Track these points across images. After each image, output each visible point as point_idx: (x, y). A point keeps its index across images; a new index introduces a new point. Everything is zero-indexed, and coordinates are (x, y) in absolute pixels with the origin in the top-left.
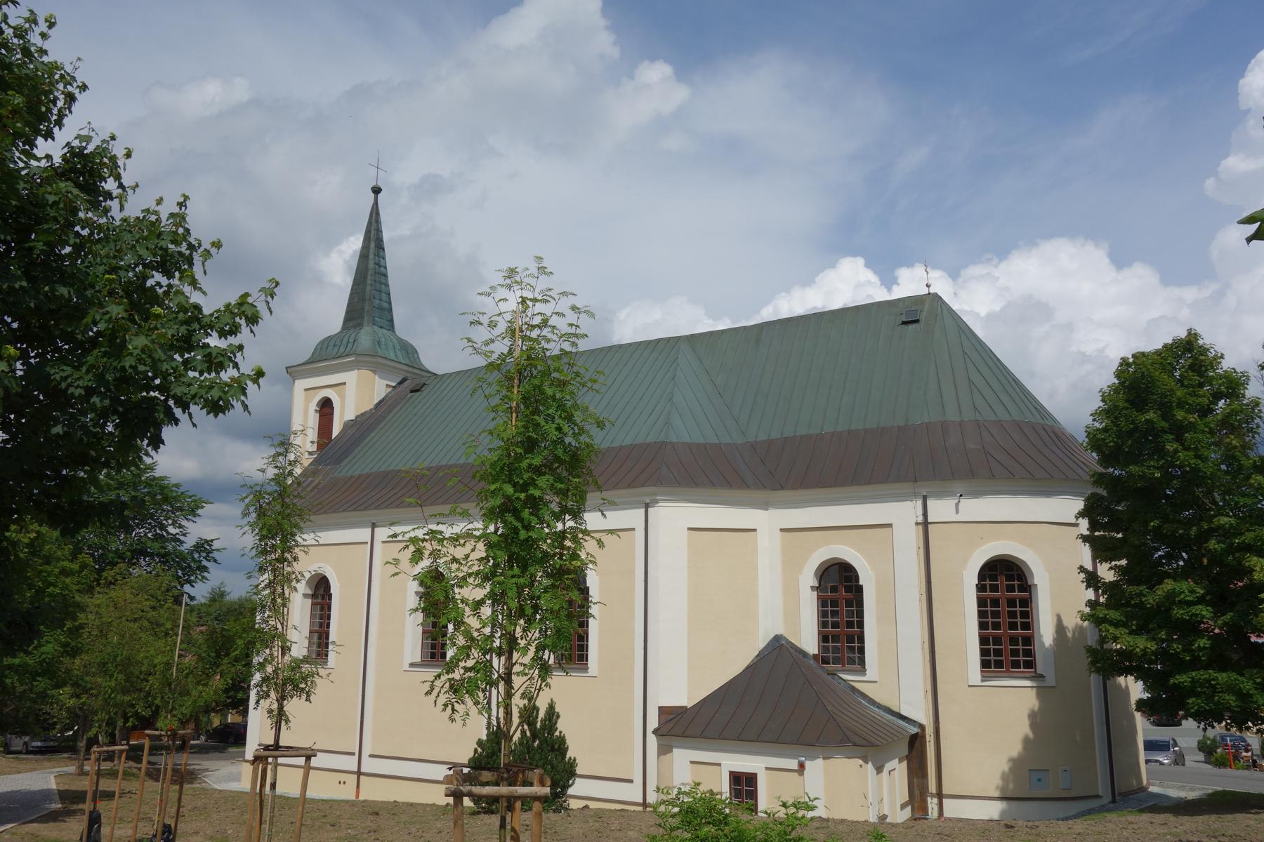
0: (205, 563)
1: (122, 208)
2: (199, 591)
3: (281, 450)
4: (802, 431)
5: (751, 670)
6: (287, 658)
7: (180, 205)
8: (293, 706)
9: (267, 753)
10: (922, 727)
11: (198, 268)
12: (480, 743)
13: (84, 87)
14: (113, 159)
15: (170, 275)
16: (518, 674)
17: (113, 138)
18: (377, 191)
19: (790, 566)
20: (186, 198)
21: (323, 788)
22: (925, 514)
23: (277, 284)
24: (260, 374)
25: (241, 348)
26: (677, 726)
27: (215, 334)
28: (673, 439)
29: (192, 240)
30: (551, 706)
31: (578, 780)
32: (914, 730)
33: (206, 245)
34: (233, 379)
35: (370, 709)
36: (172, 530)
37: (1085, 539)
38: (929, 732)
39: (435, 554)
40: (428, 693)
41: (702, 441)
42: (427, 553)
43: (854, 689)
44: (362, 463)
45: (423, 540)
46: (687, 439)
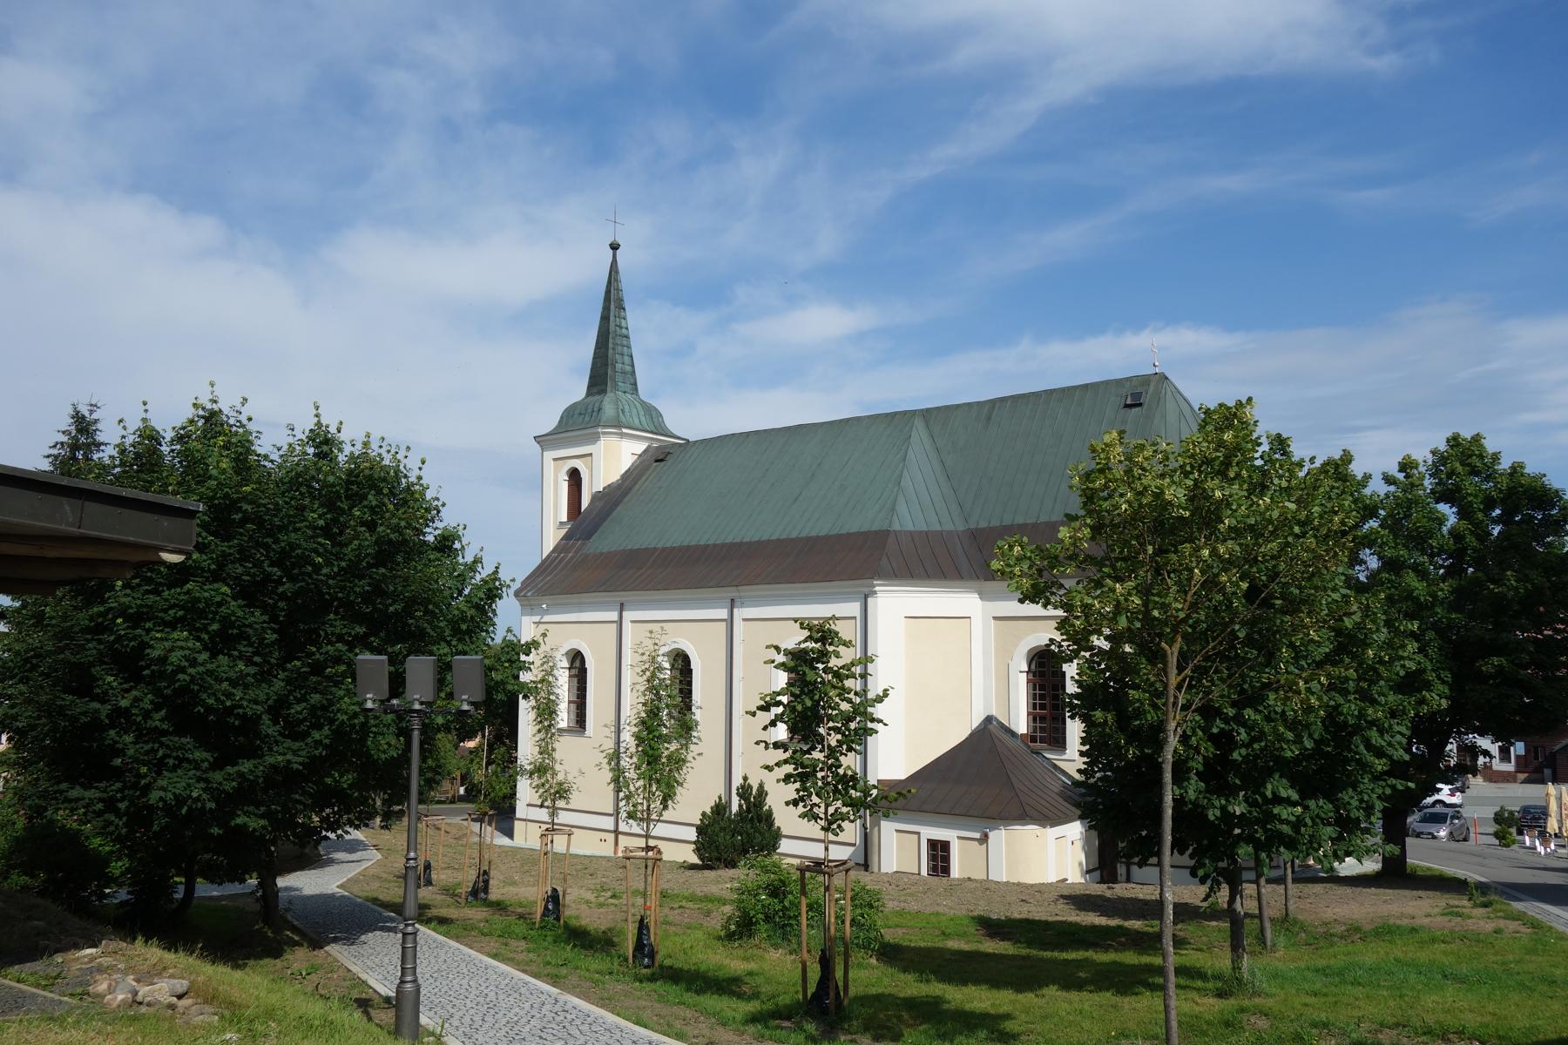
5: (295, 870)
12: (704, 814)
18: (615, 247)
19: (1004, 653)
28: (896, 527)
30: (761, 786)
41: (925, 528)
43: (1055, 766)
44: (610, 540)
46: (910, 527)
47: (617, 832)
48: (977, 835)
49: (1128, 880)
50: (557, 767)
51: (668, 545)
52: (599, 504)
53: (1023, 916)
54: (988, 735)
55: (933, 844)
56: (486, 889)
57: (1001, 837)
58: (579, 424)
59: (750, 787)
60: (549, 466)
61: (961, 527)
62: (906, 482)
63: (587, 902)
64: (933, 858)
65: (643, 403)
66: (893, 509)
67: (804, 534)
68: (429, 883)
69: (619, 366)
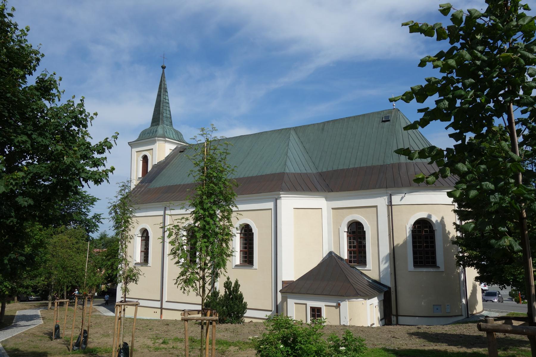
0: (97, 223)
1: (59, 100)
2: (95, 235)
3: (123, 188)
4: (341, 167)
6: (127, 268)
7: (81, 100)
8: (131, 286)
9: (121, 304)
10: (389, 288)
11: (89, 124)
13: (43, 56)
14: (55, 81)
15: (79, 127)
16: (207, 276)
17: (54, 74)
18: (164, 68)
19: (337, 223)
20: (84, 98)
21: (144, 314)
22: (391, 202)
23: (118, 134)
24: (113, 169)
25: (106, 158)
26: (291, 289)
27: (96, 153)
28: (287, 171)
29: (86, 113)
30: (237, 282)
31: (248, 311)
32: (386, 289)
33: (92, 115)
34: (103, 171)
35: (158, 290)
36: (84, 210)
37: (455, 211)
38: (393, 290)
39: (177, 234)
40: (175, 284)
41: (299, 172)
42: (174, 234)
43: (362, 273)
45: (172, 229)
46: (293, 171)
47: (161, 308)
48: (335, 304)
49: (397, 324)
50: (129, 259)
51: (186, 183)
52: (155, 169)
53: (415, 348)
54: (331, 259)
55: (313, 309)
56: (85, 342)
57: (345, 305)
58: (147, 137)
59: (231, 283)
60: (135, 154)
61: (315, 171)
62: (290, 154)
63: (148, 347)
64: (313, 315)
65: (174, 130)
66: (285, 164)
67: (246, 176)
68: (58, 337)
69: (165, 115)
